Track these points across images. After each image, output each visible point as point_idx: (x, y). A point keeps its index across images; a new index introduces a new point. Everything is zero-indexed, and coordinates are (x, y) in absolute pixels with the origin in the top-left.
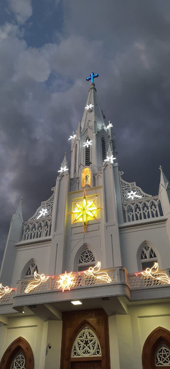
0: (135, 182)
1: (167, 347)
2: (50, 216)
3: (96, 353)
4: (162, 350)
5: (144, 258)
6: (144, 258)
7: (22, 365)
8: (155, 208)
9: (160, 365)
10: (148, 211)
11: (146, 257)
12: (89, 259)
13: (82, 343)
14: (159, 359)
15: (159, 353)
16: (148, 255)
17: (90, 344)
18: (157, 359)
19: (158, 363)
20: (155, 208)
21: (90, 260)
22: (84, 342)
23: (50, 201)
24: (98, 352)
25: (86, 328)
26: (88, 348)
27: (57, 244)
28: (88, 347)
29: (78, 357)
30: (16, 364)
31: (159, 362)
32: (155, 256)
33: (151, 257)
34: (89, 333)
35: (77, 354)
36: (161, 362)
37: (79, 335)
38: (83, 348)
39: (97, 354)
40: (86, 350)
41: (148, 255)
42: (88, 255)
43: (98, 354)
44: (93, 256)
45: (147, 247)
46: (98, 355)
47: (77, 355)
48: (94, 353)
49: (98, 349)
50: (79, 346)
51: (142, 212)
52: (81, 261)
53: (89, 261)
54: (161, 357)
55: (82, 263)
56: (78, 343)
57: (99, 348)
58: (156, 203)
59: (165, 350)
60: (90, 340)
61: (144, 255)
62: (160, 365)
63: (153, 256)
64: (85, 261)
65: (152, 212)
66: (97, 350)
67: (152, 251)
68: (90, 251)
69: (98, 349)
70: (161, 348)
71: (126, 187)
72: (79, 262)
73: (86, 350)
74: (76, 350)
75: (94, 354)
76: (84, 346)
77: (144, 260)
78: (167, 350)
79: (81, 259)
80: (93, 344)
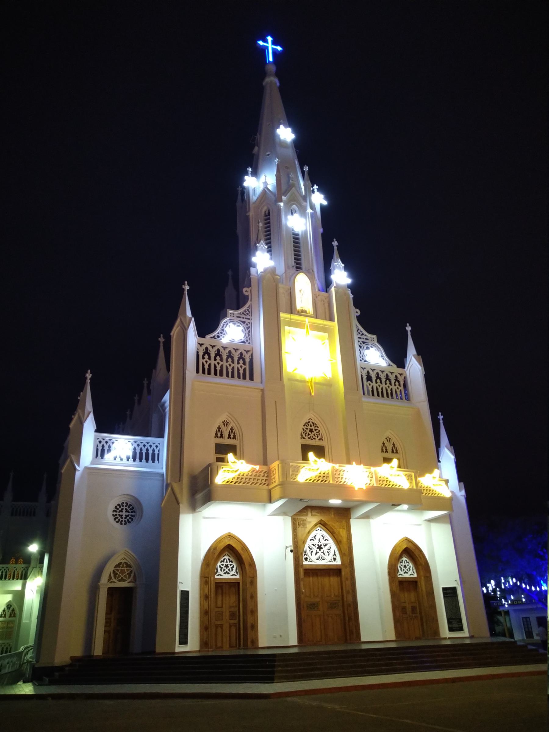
0: (228, 310)
1: (407, 557)
2: (247, 344)
3: (333, 560)
4: (402, 561)
5: (232, 438)
6: (232, 438)
7: (232, 570)
8: (243, 363)
9: (219, 577)
10: (244, 367)
11: (222, 436)
12: (316, 430)
13: (314, 547)
14: (219, 569)
15: (221, 563)
16: (226, 435)
17: (316, 549)
18: (217, 570)
19: (218, 574)
20: (220, 360)
21: (316, 438)
22: (317, 546)
23: (243, 313)
24: (335, 559)
25: (319, 530)
26: (322, 554)
27: (276, 402)
28: (322, 552)
29: (310, 563)
30: (221, 568)
31: (400, 573)
32: (234, 437)
33: (229, 437)
34: (322, 536)
35: (308, 560)
36: (222, 573)
37: (310, 538)
38: (316, 554)
39: (333, 561)
40: (320, 556)
41: (226, 435)
42: (310, 429)
43: (335, 561)
44: (320, 433)
45: (225, 422)
46: (335, 563)
47: (309, 562)
48: (312, 560)
49: (335, 556)
50: (310, 551)
51: (212, 362)
52: (304, 436)
53: (315, 439)
54: (120, 567)
55: (304, 438)
56: (309, 547)
57: (335, 555)
58: (401, 379)
59: (406, 561)
60: (324, 544)
61: (220, 433)
62: (219, 577)
63: (232, 436)
64: (316, 436)
65: (215, 366)
66: (333, 557)
67: (394, 445)
68: (306, 423)
69: (335, 556)
70: (402, 559)
71: (243, 318)
72: (321, 440)
73: (320, 556)
74: (306, 555)
75: (330, 562)
76: (317, 551)
77: (220, 441)
78: (222, 560)
79: (304, 433)
80: (329, 550)
